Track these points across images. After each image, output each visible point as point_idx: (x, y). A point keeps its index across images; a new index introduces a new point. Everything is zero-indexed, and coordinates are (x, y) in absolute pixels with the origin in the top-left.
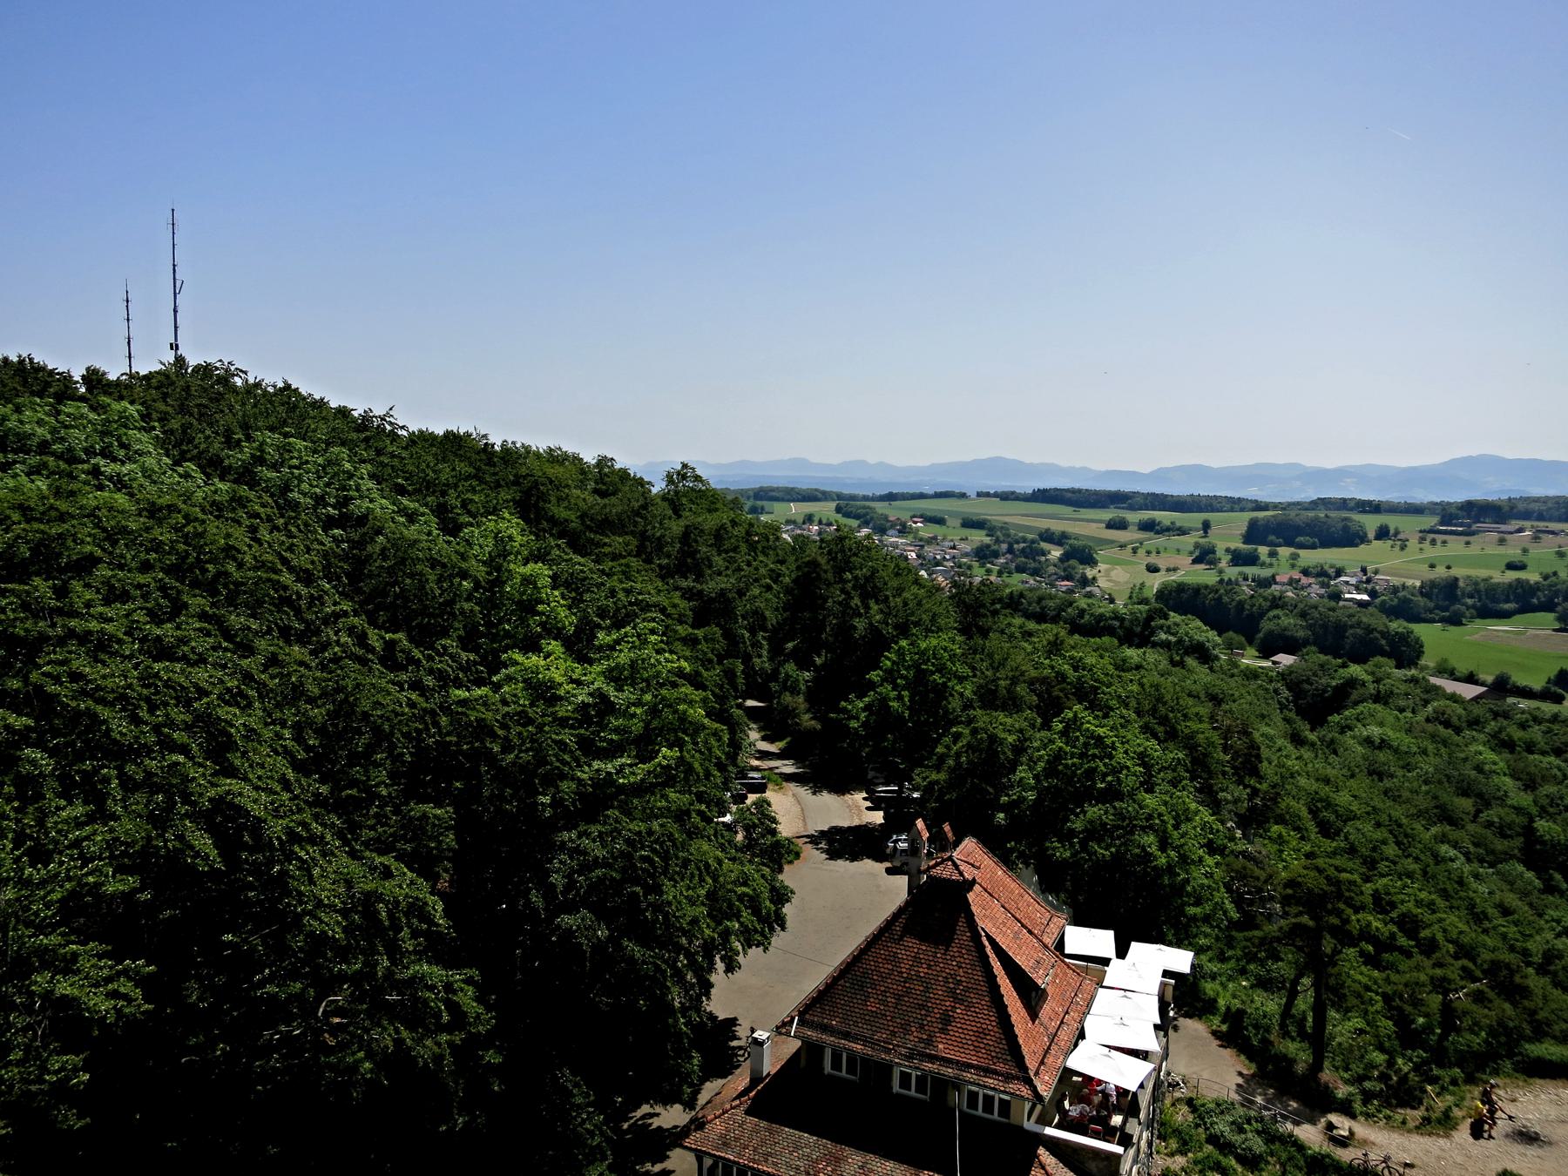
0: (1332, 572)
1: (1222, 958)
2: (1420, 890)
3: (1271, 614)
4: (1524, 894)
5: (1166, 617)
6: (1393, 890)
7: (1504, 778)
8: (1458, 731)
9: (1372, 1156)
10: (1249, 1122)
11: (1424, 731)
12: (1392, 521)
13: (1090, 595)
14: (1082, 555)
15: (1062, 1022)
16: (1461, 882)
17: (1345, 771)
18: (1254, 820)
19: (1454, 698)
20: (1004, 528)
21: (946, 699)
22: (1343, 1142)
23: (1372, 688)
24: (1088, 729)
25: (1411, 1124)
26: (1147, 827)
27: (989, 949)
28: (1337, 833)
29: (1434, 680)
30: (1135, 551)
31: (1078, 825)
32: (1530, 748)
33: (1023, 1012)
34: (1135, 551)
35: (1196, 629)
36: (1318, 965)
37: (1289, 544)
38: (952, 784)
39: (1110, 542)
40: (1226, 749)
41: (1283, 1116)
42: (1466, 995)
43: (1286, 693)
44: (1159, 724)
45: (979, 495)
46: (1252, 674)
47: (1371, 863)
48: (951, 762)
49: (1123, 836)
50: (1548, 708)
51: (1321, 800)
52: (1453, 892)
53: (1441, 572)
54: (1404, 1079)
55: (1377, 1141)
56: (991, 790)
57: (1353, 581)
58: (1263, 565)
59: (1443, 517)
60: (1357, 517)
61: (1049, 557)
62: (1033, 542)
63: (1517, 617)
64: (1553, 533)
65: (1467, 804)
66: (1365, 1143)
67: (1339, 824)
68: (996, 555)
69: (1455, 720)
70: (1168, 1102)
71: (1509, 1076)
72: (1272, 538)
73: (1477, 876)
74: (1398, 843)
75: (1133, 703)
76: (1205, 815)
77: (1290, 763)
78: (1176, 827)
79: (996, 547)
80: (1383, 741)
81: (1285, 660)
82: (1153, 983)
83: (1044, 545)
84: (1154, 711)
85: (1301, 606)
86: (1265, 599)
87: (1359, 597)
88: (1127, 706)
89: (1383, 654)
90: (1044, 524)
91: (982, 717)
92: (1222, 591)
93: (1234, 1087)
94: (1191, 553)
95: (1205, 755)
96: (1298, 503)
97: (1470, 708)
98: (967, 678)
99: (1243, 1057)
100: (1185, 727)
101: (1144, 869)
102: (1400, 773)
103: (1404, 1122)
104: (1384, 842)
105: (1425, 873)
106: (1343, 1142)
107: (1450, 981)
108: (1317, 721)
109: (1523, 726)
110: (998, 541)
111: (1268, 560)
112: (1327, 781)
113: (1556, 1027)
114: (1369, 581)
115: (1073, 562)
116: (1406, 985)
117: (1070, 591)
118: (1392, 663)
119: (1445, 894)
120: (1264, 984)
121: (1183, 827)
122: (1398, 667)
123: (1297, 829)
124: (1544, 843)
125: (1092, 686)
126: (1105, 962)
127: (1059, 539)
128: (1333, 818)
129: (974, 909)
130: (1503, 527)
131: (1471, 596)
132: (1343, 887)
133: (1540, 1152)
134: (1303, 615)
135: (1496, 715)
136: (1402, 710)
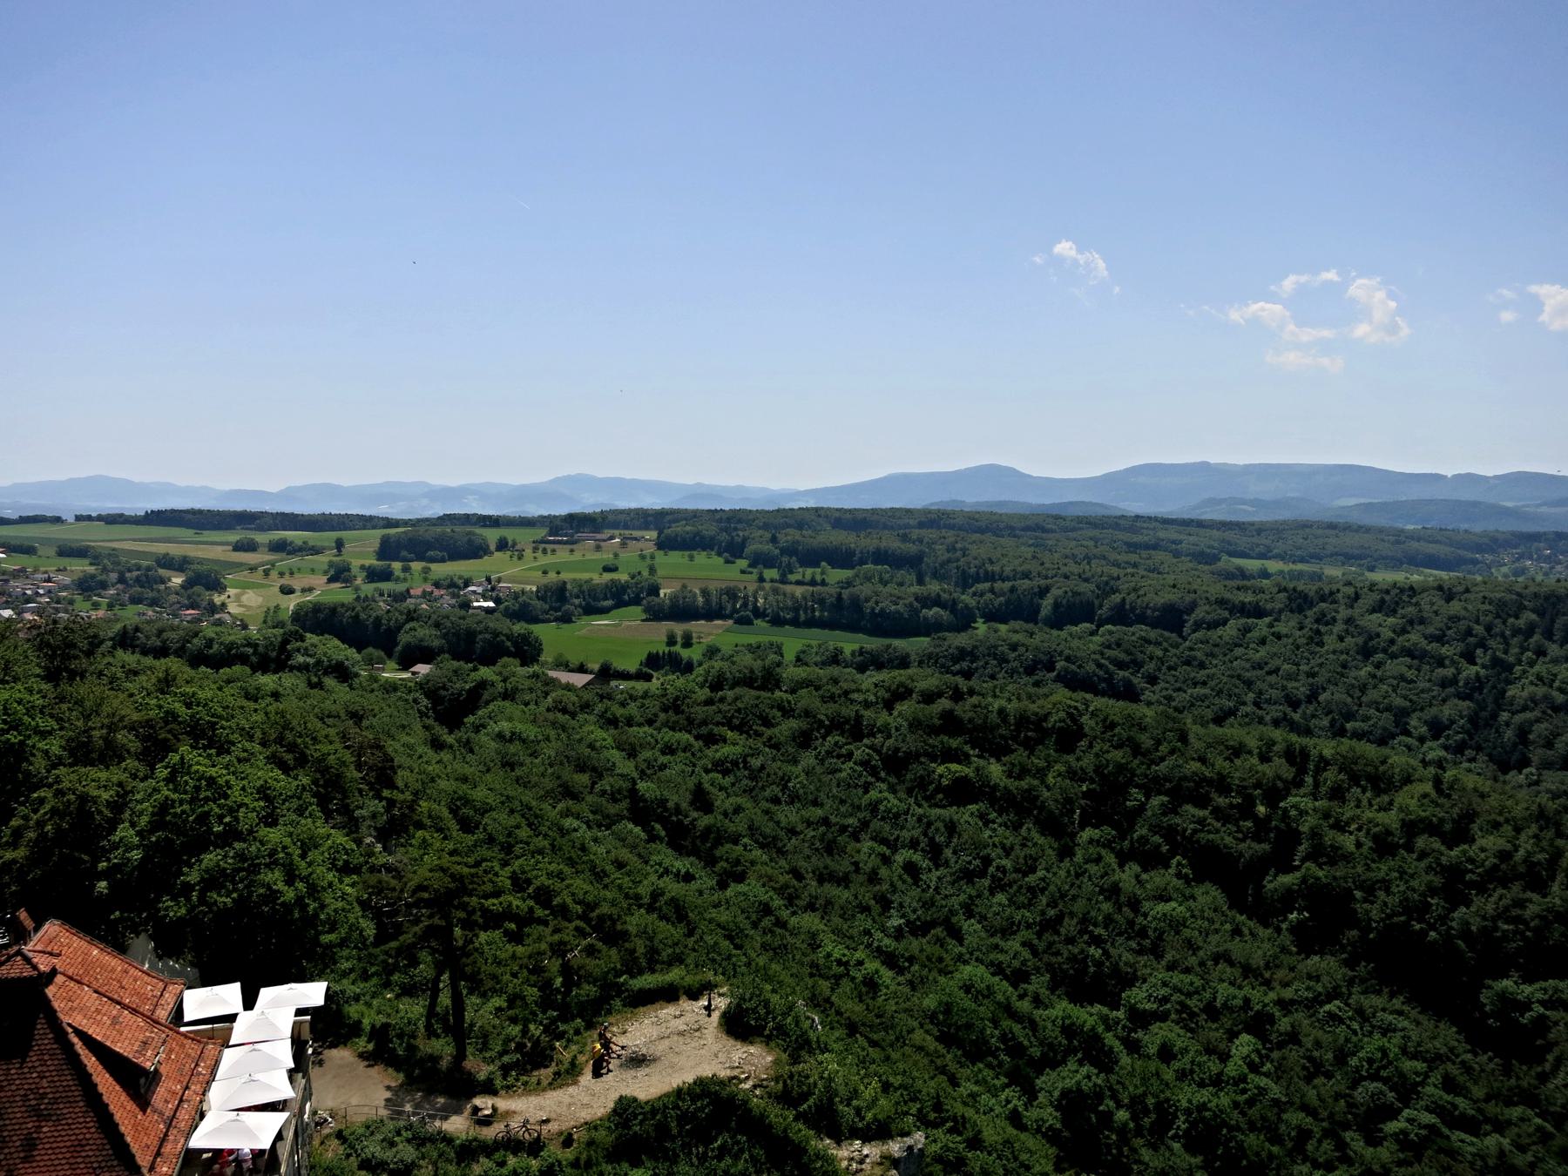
0: (460, 583)
1: (365, 977)
2: (550, 863)
3: (407, 626)
4: (634, 847)
5: (302, 639)
6: (527, 869)
7: (612, 751)
8: (573, 715)
9: (514, 1125)
10: (399, 1133)
11: (546, 720)
12: (510, 534)
13: (220, 623)
14: (207, 580)
15: (181, 1101)
16: (583, 849)
17: (481, 768)
18: (394, 829)
19: (569, 687)
20: (113, 554)
21: (27, 760)
22: (486, 1122)
23: (500, 687)
24: (197, 771)
25: (545, 1083)
26: (271, 863)
27: (90, 1062)
28: (477, 827)
29: (553, 674)
30: (267, 573)
31: (193, 877)
32: (630, 722)
33: (131, 1105)
34: (267, 573)
35: (333, 648)
36: (454, 960)
37: (420, 558)
38: (35, 859)
39: (238, 566)
40: (359, 767)
41: (430, 1116)
42: (580, 952)
43: (425, 701)
44: (288, 751)
45: (79, 518)
46: (391, 687)
47: (508, 848)
48: (32, 835)
49: (246, 878)
50: (640, 686)
51: (460, 798)
52: (577, 859)
53: (552, 576)
54: (537, 1043)
55: (518, 1109)
56: (86, 858)
57: (480, 590)
58: (397, 580)
59: (551, 529)
60: (478, 530)
61: (170, 584)
62: (149, 569)
63: (614, 612)
64: (636, 539)
65: (584, 779)
66: (509, 1114)
67: (477, 817)
68: (104, 585)
69: (570, 708)
70: (316, 1142)
71: (619, 1012)
72: (404, 553)
73: (596, 840)
74: (530, 825)
75: (258, 734)
76: (340, 838)
77: (431, 768)
78: (303, 856)
79: (104, 577)
80: (513, 734)
81: (423, 669)
82: (285, 1022)
83: (162, 572)
84: (280, 740)
85: (434, 617)
86: (401, 613)
87: (485, 604)
88: (251, 738)
89: (510, 654)
90: (161, 548)
91: (67, 776)
92: (358, 608)
93: (383, 1103)
94: (325, 573)
95: (339, 776)
96: (427, 520)
97: (581, 694)
98: (50, 733)
99: (390, 1070)
100: (313, 752)
101: (273, 908)
102: (528, 760)
103: (539, 1083)
104: (518, 827)
105: (553, 846)
106: (486, 1122)
107: (565, 944)
108: (453, 722)
109: (623, 704)
110: (105, 570)
111: (402, 575)
112: (465, 779)
113: (664, 954)
114: (493, 589)
115: (198, 589)
116: (530, 957)
117: (198, 620)
118: (517, 662)
119: (571, 862)
120: (408, 991)
121: (311, 856)
122: (522, 665)
123: (440, 830)
124: (645, 801)
125: (209, 722)
126: (232, 1018)
127: (180, 565)
128: (472, 813)
129: (56, 1005)
130: (598, 536)
131: (578, 597)
132: (466, 881)
133: (647, 1070)
134: (437, 625)
135: (602, 697)
136: (526, 704)
